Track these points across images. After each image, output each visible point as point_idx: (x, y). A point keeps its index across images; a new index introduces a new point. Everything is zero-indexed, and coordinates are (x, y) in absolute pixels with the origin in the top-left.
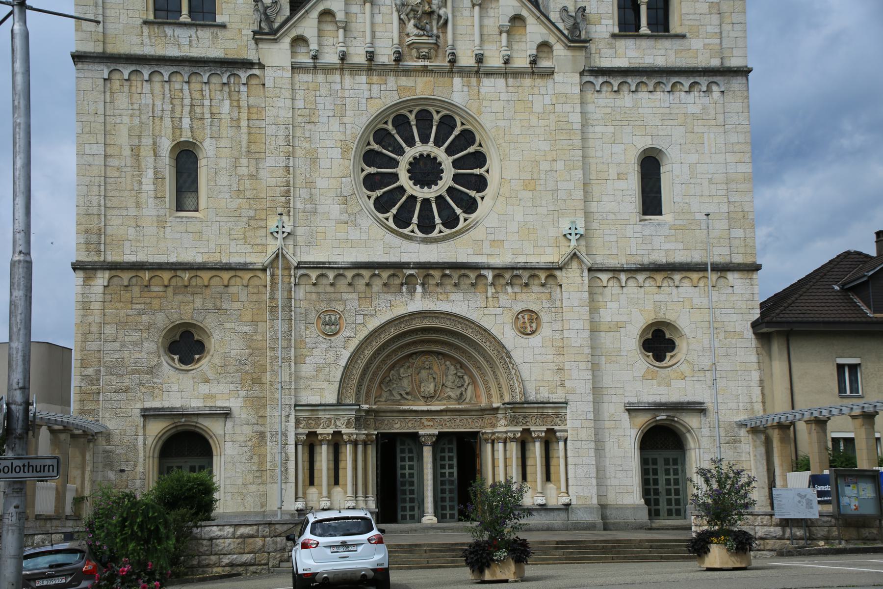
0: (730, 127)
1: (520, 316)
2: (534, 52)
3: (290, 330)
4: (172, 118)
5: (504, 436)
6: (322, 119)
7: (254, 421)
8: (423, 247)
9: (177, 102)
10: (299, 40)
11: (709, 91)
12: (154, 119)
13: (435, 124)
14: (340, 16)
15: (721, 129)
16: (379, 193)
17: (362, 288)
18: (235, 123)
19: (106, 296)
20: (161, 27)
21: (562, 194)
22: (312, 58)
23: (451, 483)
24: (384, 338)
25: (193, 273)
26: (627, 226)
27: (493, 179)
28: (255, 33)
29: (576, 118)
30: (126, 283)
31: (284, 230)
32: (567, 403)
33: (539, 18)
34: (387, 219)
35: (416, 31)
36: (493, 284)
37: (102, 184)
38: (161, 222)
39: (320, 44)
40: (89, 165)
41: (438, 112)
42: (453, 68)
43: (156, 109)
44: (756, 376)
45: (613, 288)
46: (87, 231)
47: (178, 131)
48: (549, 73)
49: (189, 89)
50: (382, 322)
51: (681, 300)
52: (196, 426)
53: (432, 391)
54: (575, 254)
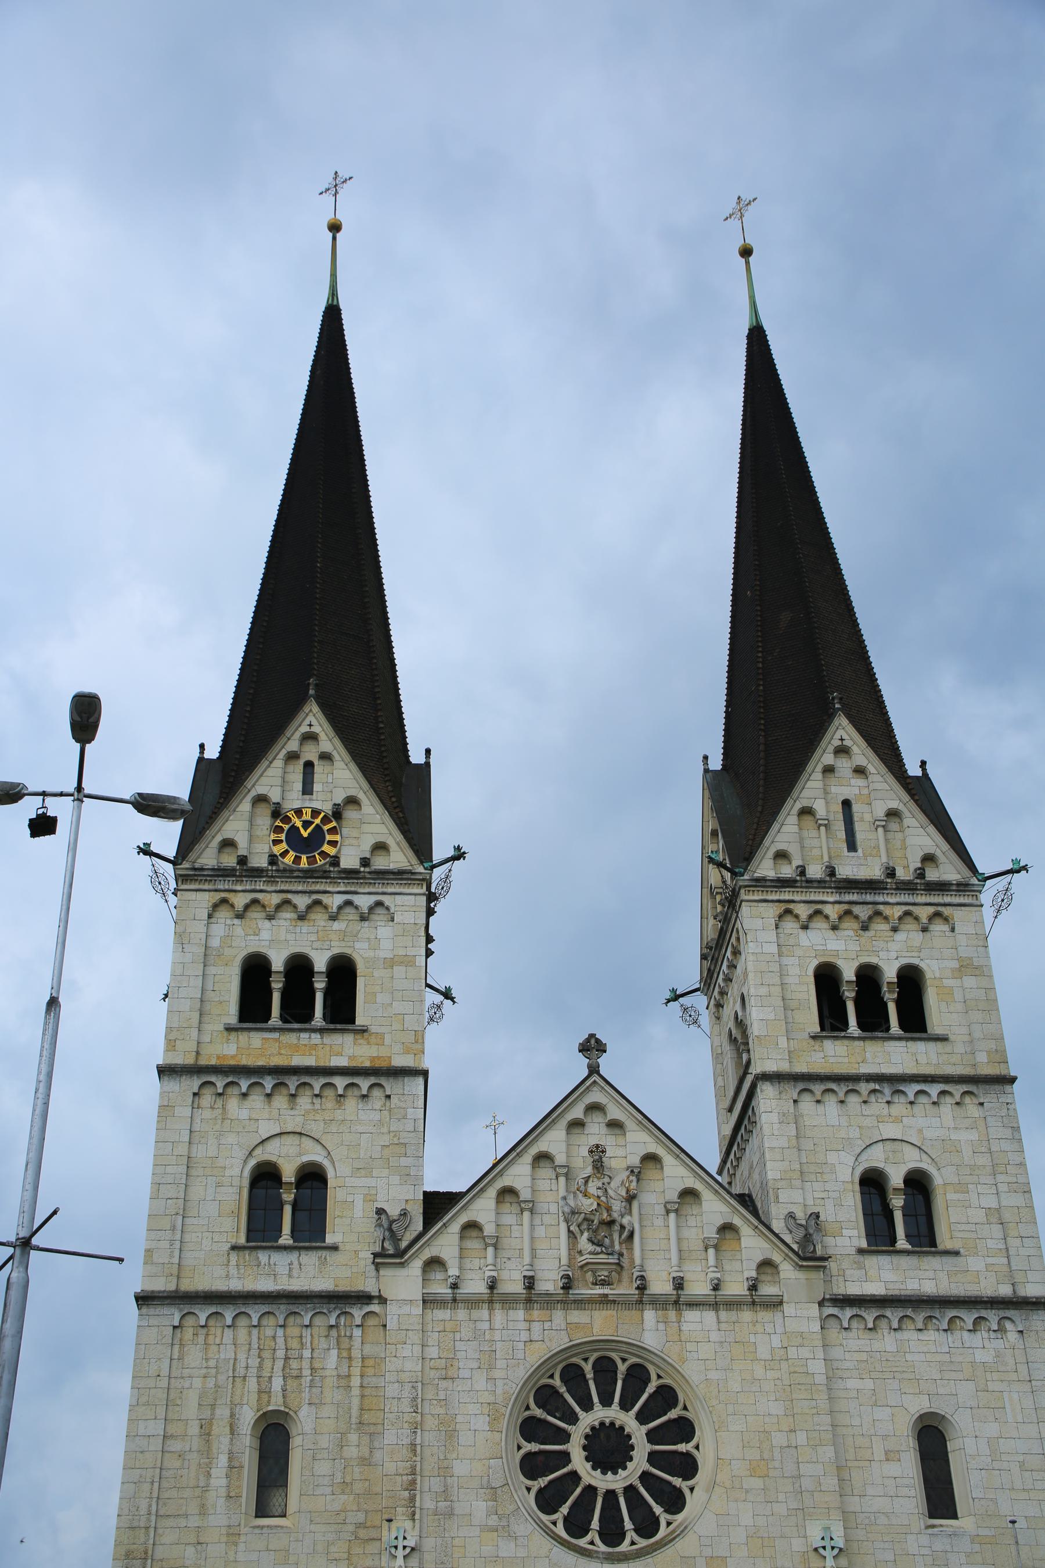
0: (1039, 1383)
2: (754, 1274)
4: (259, 1377)
6: (463, 1373)
9: (266, 1354)
10: (435, 1263)
11: (1001, 1330)
12: (234, 1381)
13: (620, 1377)
14: (489, 1229)
15: (1027, 1387)
16: (543, 1482)
18: (343, 1382)
20: (254, 1253)
21: (807, 1483)
22: (451, 1288)
26: (909, 1537)
27: (705, 1459)
28: (376, 1255)
29: (817, 1367)
31: (406, 1543)
33: (756, 1227)
34: (554, 1523)
35: (590, 1247)
37: (157, 1479)
39: (461, 1268)
40: (142, 1452)
41: (624, 1360)
46: (128, 1555)
47: (265, 1397)
48: (776, 1304)
49: (285, 1336)
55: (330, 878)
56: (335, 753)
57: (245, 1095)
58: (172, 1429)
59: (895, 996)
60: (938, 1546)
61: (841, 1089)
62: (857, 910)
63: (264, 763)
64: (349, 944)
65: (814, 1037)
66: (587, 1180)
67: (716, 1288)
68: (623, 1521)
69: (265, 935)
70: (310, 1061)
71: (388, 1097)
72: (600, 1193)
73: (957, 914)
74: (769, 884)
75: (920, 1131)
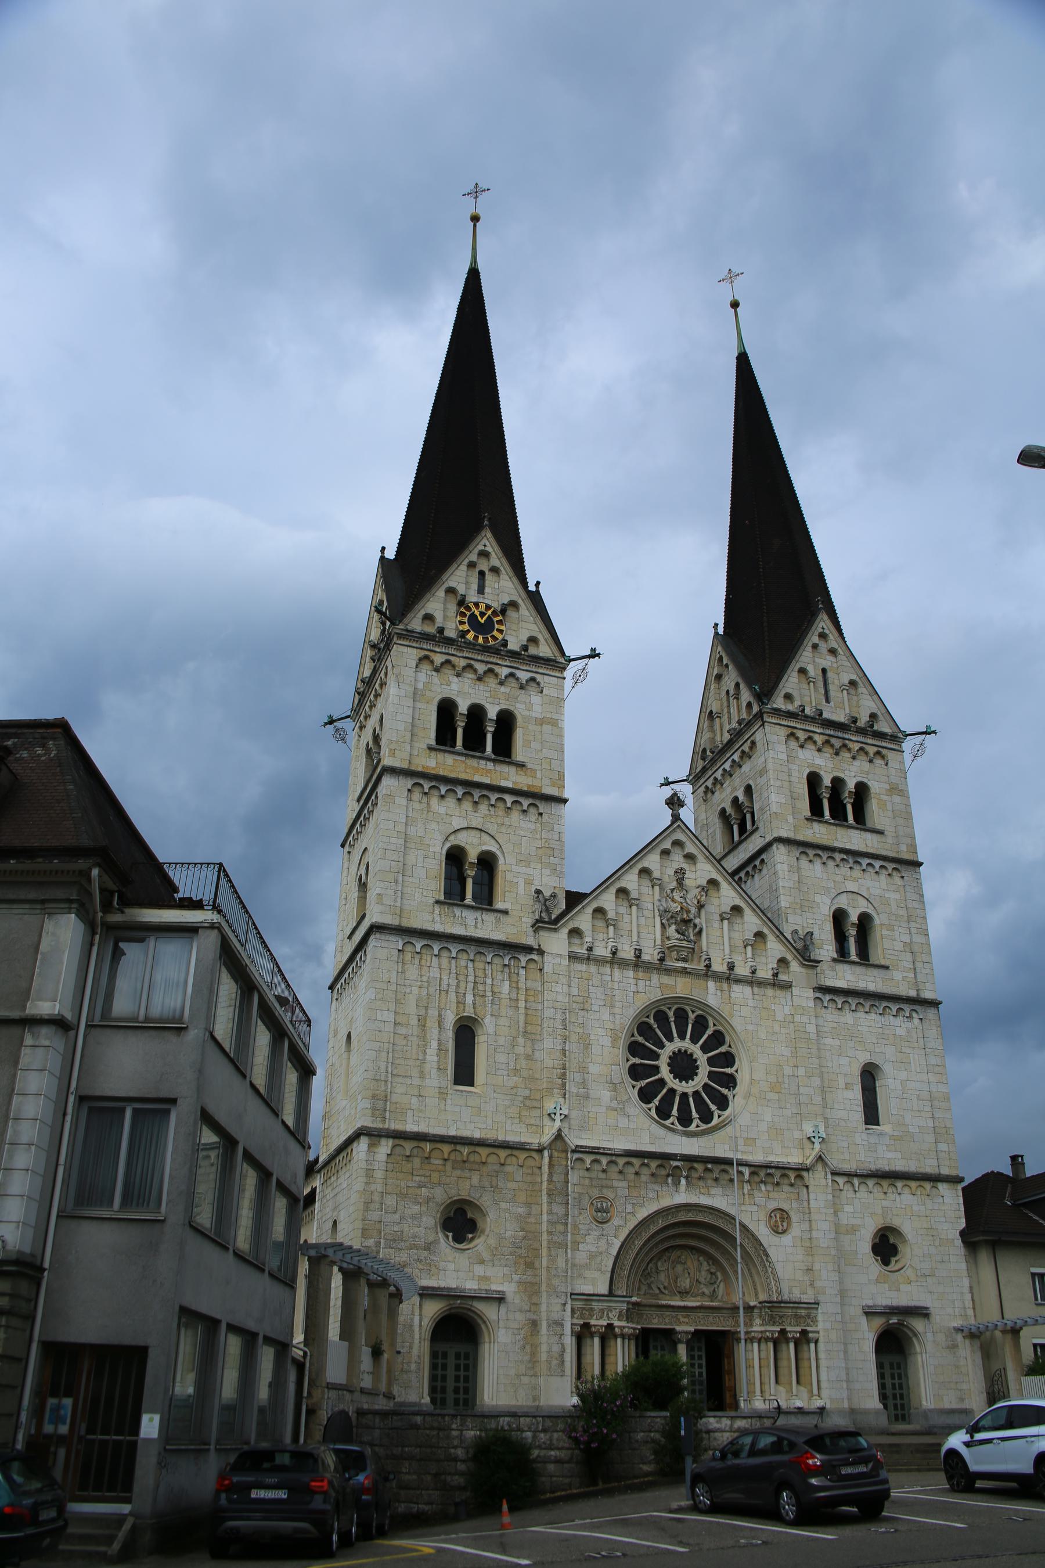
0: (930, 1050)
1: (772, 1215)
3: (567, 1215)
4: (457, 992)
5: (760, 1336)
7: (527, 1308)
8: (685, 1139)
9: (462, 978)
10: (575, 932)
12: (440, 993)
14: (611, 915)
15: (922, 1052)
17: (632, 1177)
18: (513, 1004)
19: (389, 1165)
20: (451, 908)
21: (803, 1099)
22: (587, 950)
23: (701, 1383)
24: (653, 1229)
25: (472, 1148)
26: (856, 1134)
29: (811, 1029)
30: (408, 1154)
32: (818, 1304)
33: (778, 936)
34: (650, 1110)
35: (678, 936)
36: (749, 1181)
37: (391, 1050)
38: (442, 1094)
40: (380, 1031)
41: (693, 1012)
42: (708, 973)
43: (442, 983)
44: (966, 1282)
45: (848, 1193)
48: (787, 986)
50: (651, 1212)
51: (903, 1206)
52: (469, 1310)
53: (688, 1287)
54: (820, 1157)
55: (500, 655)
56: (502, 568)
57: (442, 797)
58: (400, 1019)
59: (852, 801)
60: (872, 1140)
61: (825, 855)
62: (833, 741)
63: (455, 566)
64: (511, 703)
65: (807, 819)
66: (672, 890)
67: (753, 972)
68: (691, 1112)
69: (454, 686)
70: (486, 780)
71: (541, 814)
72: (682, 900)
73: (890, 755)
74: (782, 713)
75: (868, 889)
